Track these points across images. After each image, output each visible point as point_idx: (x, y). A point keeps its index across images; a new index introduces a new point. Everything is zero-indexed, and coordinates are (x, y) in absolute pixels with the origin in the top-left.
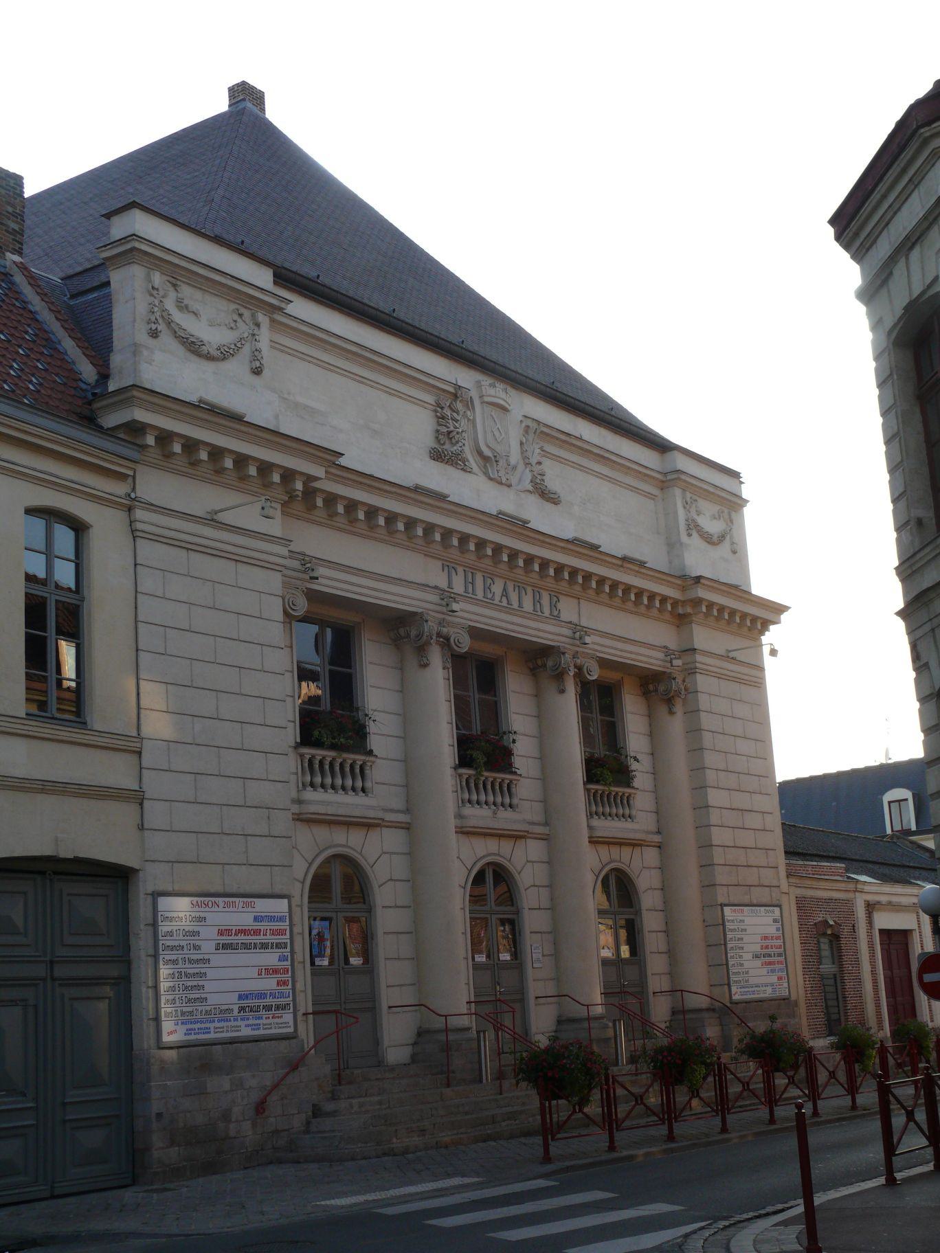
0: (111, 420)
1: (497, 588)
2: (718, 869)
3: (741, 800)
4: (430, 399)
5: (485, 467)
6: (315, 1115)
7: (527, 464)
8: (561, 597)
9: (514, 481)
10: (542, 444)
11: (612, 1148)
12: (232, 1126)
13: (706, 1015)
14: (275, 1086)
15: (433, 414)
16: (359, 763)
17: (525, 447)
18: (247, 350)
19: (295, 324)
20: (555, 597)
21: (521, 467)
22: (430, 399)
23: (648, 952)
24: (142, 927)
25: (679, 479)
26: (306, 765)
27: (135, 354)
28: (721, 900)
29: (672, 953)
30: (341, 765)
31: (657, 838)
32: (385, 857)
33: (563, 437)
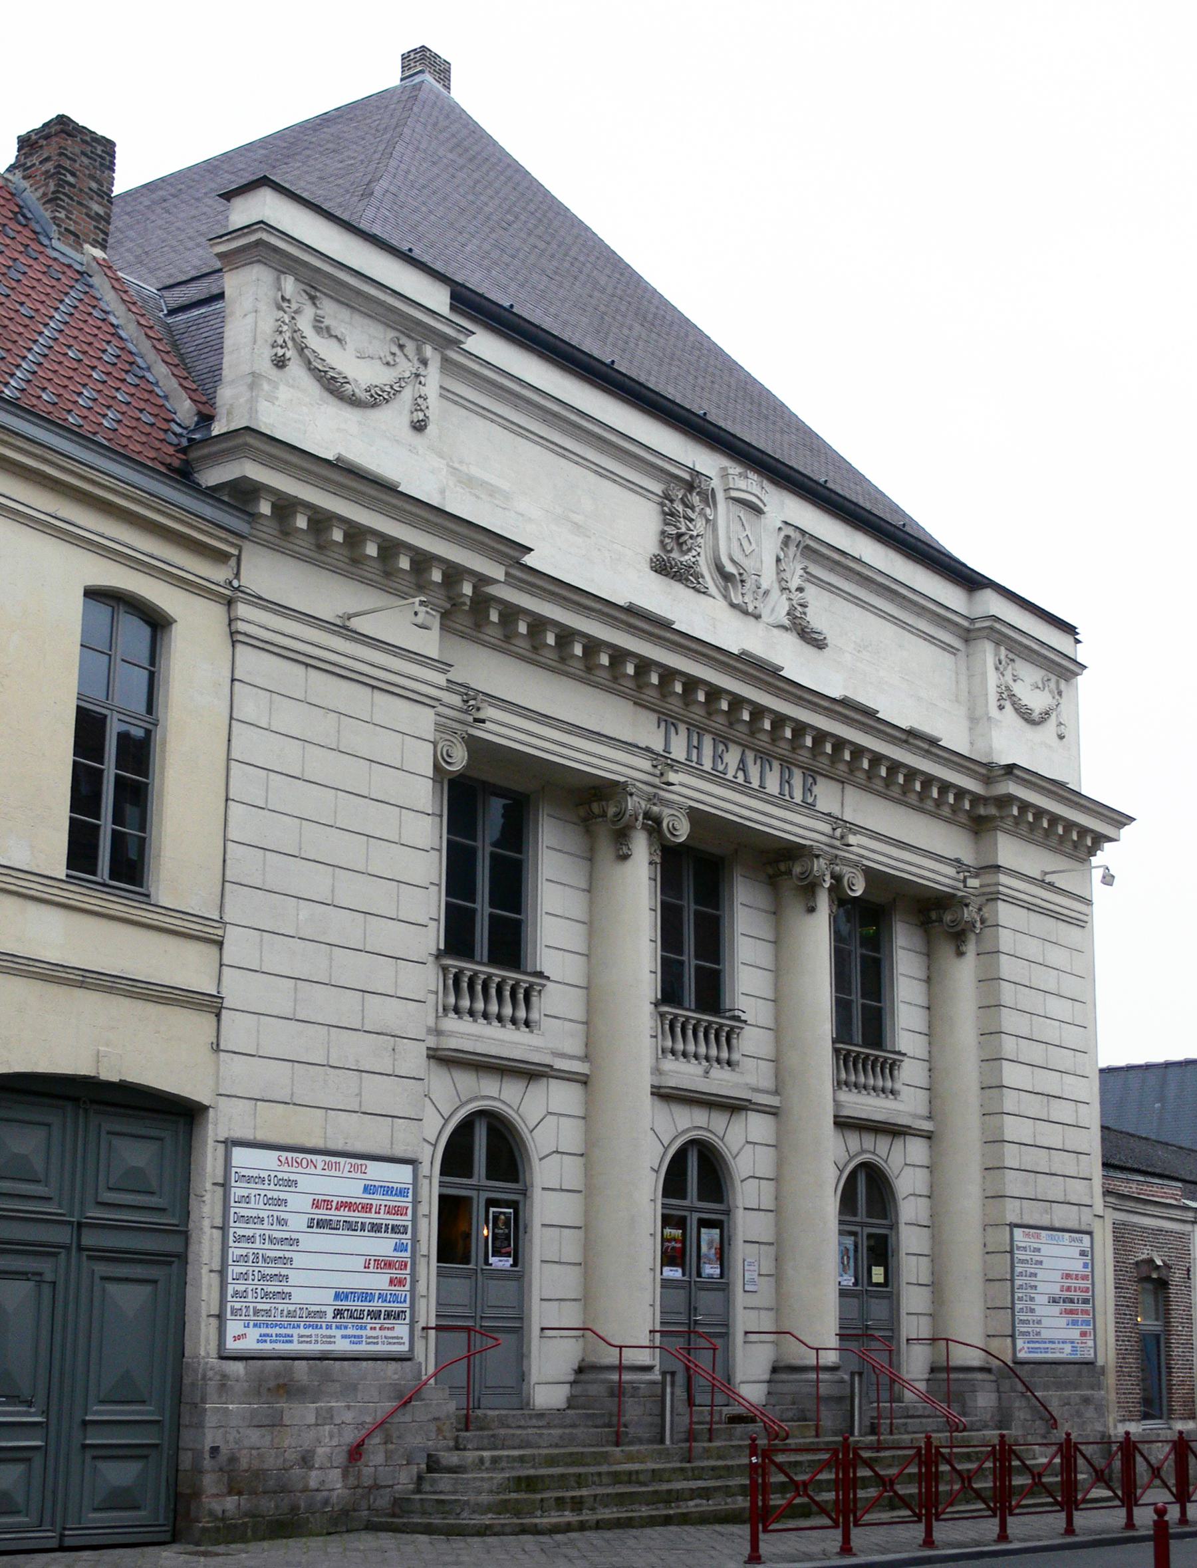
0: (213, 476)
3: (1049, 1082)
4: (657, 488)
5: (726, 588)
6: (430, 1469)
8: (819, 779)
10: (807, 563)
13: (979, 1376)
15: (658, 508)
17: (783, 566)
18: (407, 395)
24: (208, 1186)
28: (1012, 1218)
29: (936, 1286)
33: (836, 556)
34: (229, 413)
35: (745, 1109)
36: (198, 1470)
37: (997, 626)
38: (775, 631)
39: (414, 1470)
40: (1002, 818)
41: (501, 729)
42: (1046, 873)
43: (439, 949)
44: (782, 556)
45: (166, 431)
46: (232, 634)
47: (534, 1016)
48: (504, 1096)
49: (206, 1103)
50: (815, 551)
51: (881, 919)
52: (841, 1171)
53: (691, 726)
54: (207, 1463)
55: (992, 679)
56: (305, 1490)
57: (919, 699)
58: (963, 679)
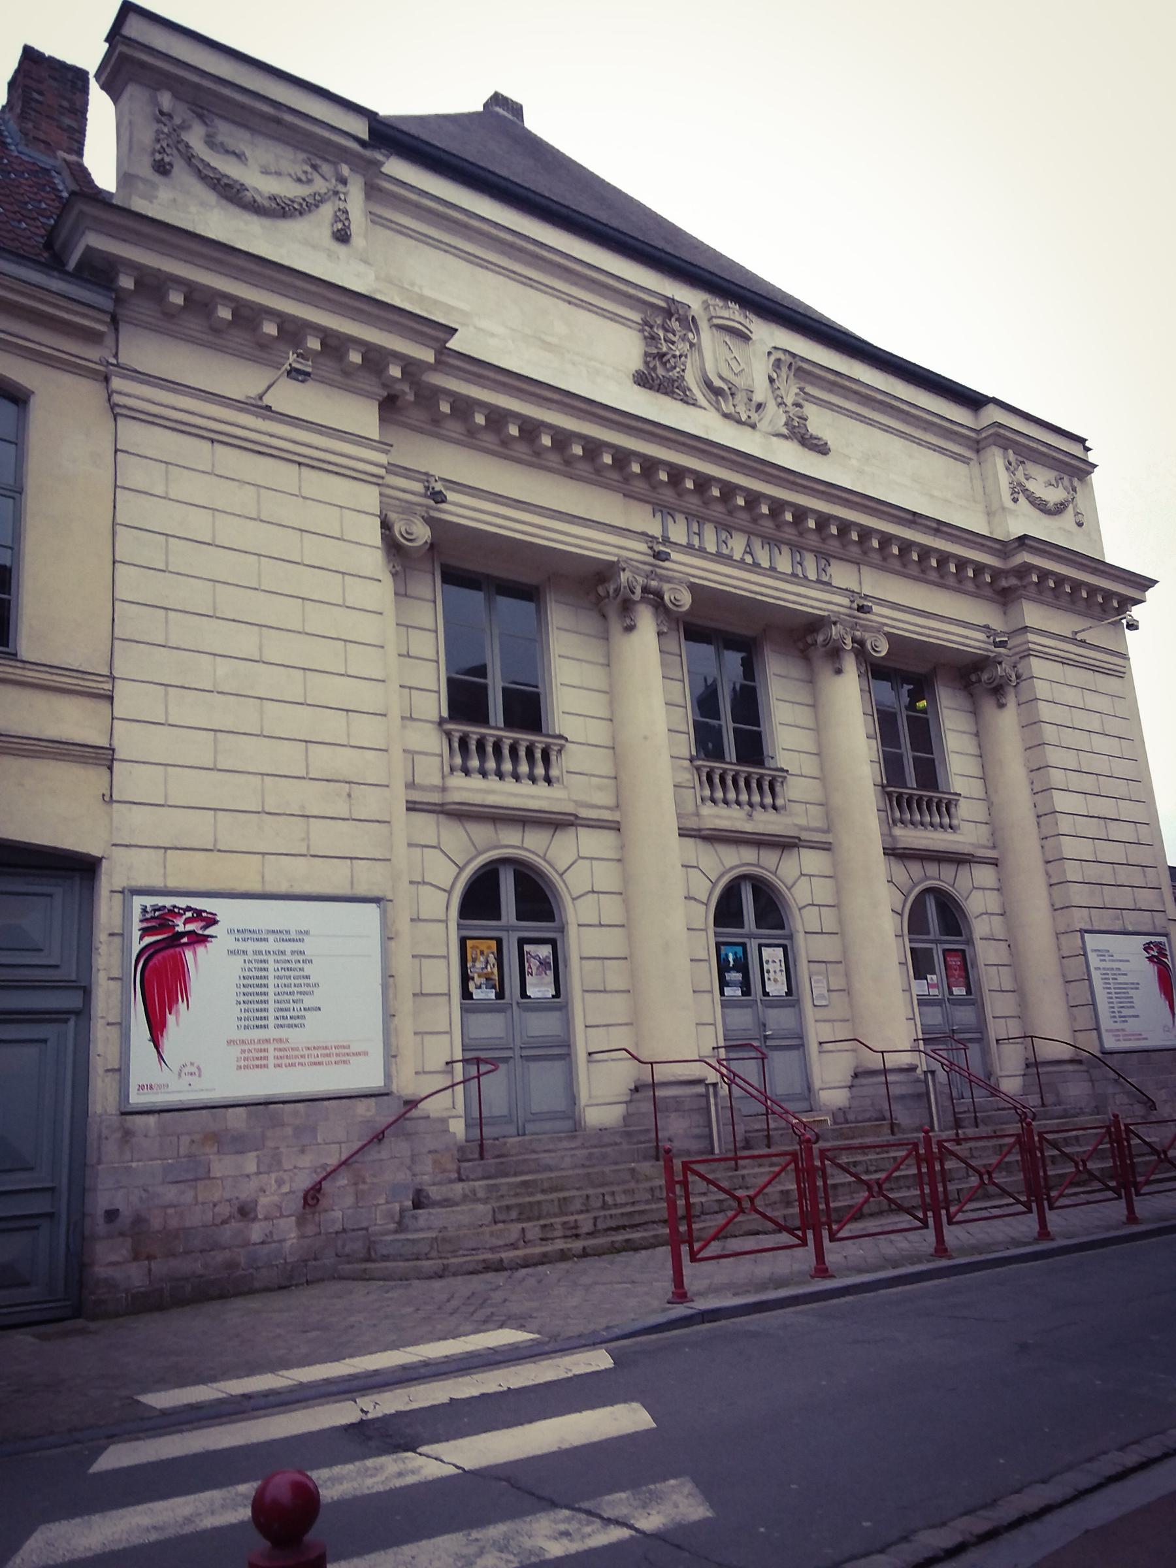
4: (636, 317)
5: (718, 402)
6: (417, 1205)
8: (832, 561)
10: (802, 385)
13: (1070, 1067)
17: (777, 384)
19: (413, 197)
26: (456, 745)
32: (580, 861)
35: (795, 846)
37: (1002, 431)
38: (775, 439)
40: (1025, 587)
42: (1076, 633)
43: (441, 717)
44: (775, 376)
46: (112, 409)
48: (766, 863)
49: (96, 852)
50: (809, 373)
51: (912, 683)
52: (906, 897)
53: (689, 516)
55: (1004, 478)
56: (246, 1244)
57: (932, 496)
58: (978, 483)
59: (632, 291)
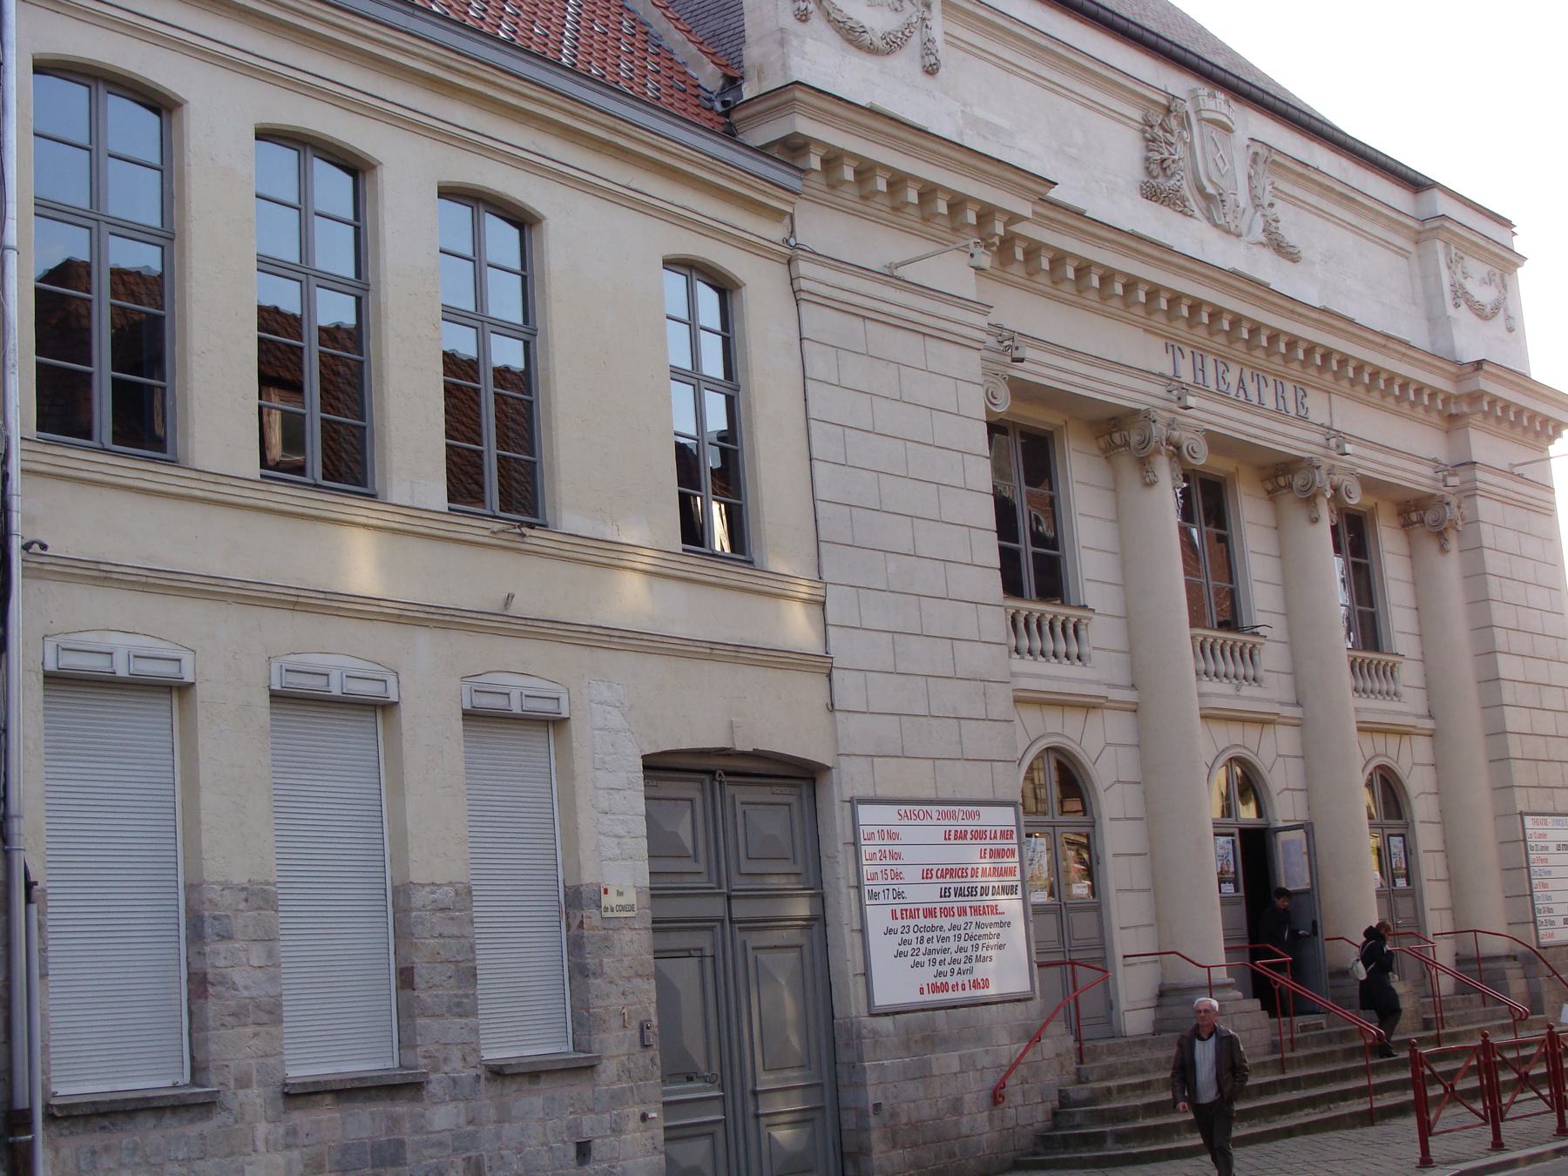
0: (762, 135)
1: (1232, 377)
2: (1516, 766)
3: (1538, 671)
4: (1137, 114)
7: (1257, 206)
8: (1308, 391)
9: (1244, 229)
10: (1273, 178)
11: (1498, 1145)
12: (965, 1120)
13: (1508, 964)
14: (1013, 1067)
15: (1140, 135)
16: (1049, 617)
18: (916, 40)
20: (1302, 387)
21: (1250, 210)
22: (1137, 114)
23: (1424, 881)
24: (840, 847)
25: (1441, 227)
27: (782, 43)
28: (1521, 807)
29: (1453, 880)
30: (1051, 624)
31: (1428, 724)
33: (1299, 169)
34: (760, 72)
36: (863, 1128)
39: (1049, 1106)
41: (1040, 369)
45: (697, 96)
47: (1086, 650)
54: (873, 1121)
59: (1139, 89)
